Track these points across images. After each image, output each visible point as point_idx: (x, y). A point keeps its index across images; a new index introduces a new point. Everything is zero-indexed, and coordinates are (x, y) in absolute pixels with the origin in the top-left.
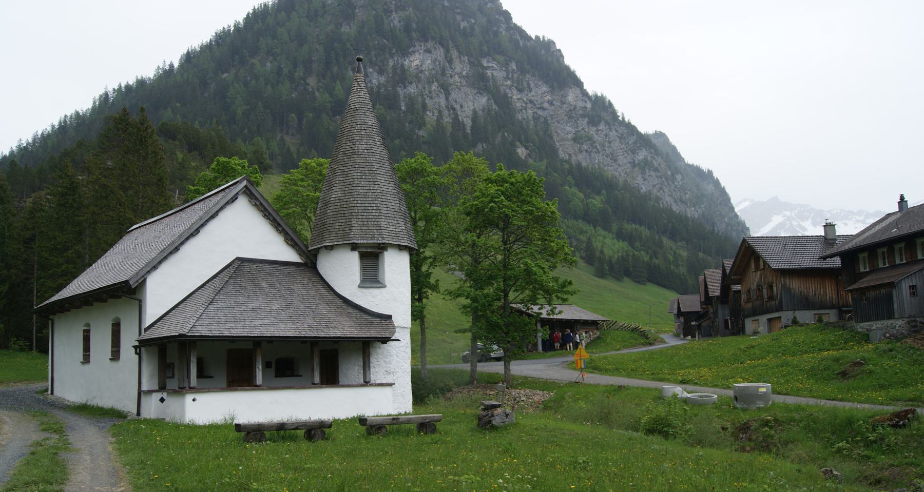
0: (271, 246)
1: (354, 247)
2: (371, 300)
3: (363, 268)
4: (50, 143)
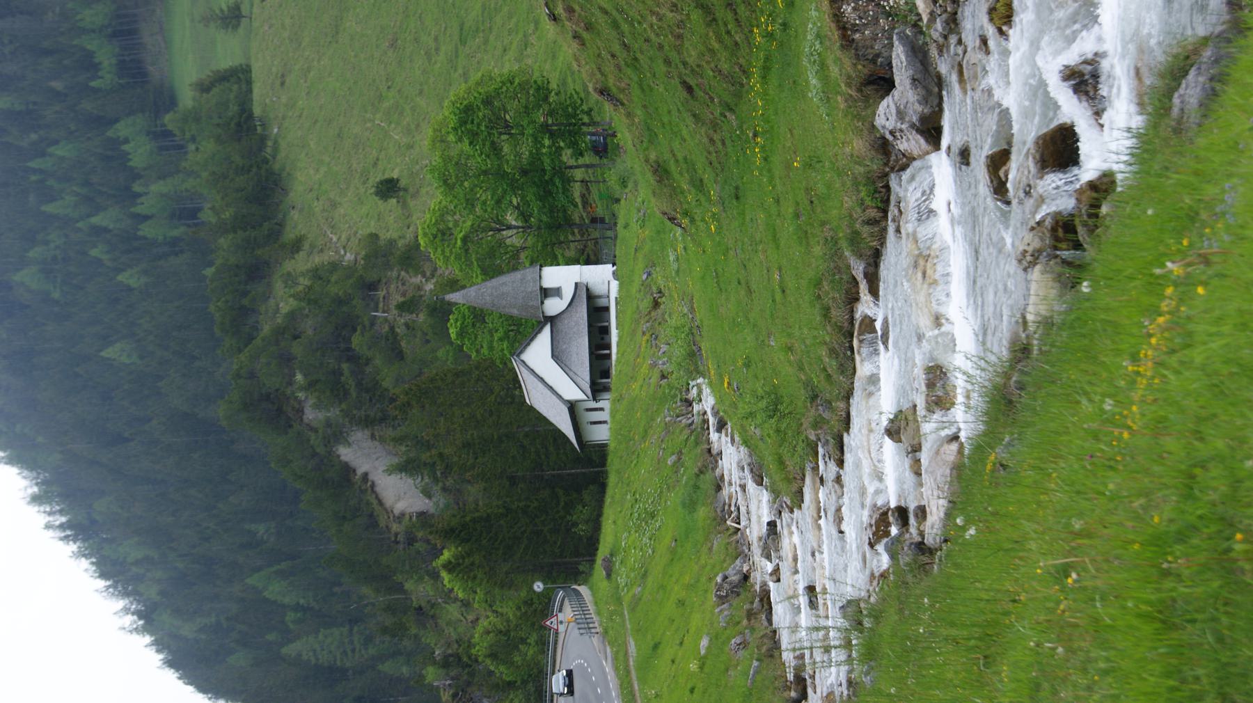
0: (543, 341)
2: (568, 293)
4: (132, 550)
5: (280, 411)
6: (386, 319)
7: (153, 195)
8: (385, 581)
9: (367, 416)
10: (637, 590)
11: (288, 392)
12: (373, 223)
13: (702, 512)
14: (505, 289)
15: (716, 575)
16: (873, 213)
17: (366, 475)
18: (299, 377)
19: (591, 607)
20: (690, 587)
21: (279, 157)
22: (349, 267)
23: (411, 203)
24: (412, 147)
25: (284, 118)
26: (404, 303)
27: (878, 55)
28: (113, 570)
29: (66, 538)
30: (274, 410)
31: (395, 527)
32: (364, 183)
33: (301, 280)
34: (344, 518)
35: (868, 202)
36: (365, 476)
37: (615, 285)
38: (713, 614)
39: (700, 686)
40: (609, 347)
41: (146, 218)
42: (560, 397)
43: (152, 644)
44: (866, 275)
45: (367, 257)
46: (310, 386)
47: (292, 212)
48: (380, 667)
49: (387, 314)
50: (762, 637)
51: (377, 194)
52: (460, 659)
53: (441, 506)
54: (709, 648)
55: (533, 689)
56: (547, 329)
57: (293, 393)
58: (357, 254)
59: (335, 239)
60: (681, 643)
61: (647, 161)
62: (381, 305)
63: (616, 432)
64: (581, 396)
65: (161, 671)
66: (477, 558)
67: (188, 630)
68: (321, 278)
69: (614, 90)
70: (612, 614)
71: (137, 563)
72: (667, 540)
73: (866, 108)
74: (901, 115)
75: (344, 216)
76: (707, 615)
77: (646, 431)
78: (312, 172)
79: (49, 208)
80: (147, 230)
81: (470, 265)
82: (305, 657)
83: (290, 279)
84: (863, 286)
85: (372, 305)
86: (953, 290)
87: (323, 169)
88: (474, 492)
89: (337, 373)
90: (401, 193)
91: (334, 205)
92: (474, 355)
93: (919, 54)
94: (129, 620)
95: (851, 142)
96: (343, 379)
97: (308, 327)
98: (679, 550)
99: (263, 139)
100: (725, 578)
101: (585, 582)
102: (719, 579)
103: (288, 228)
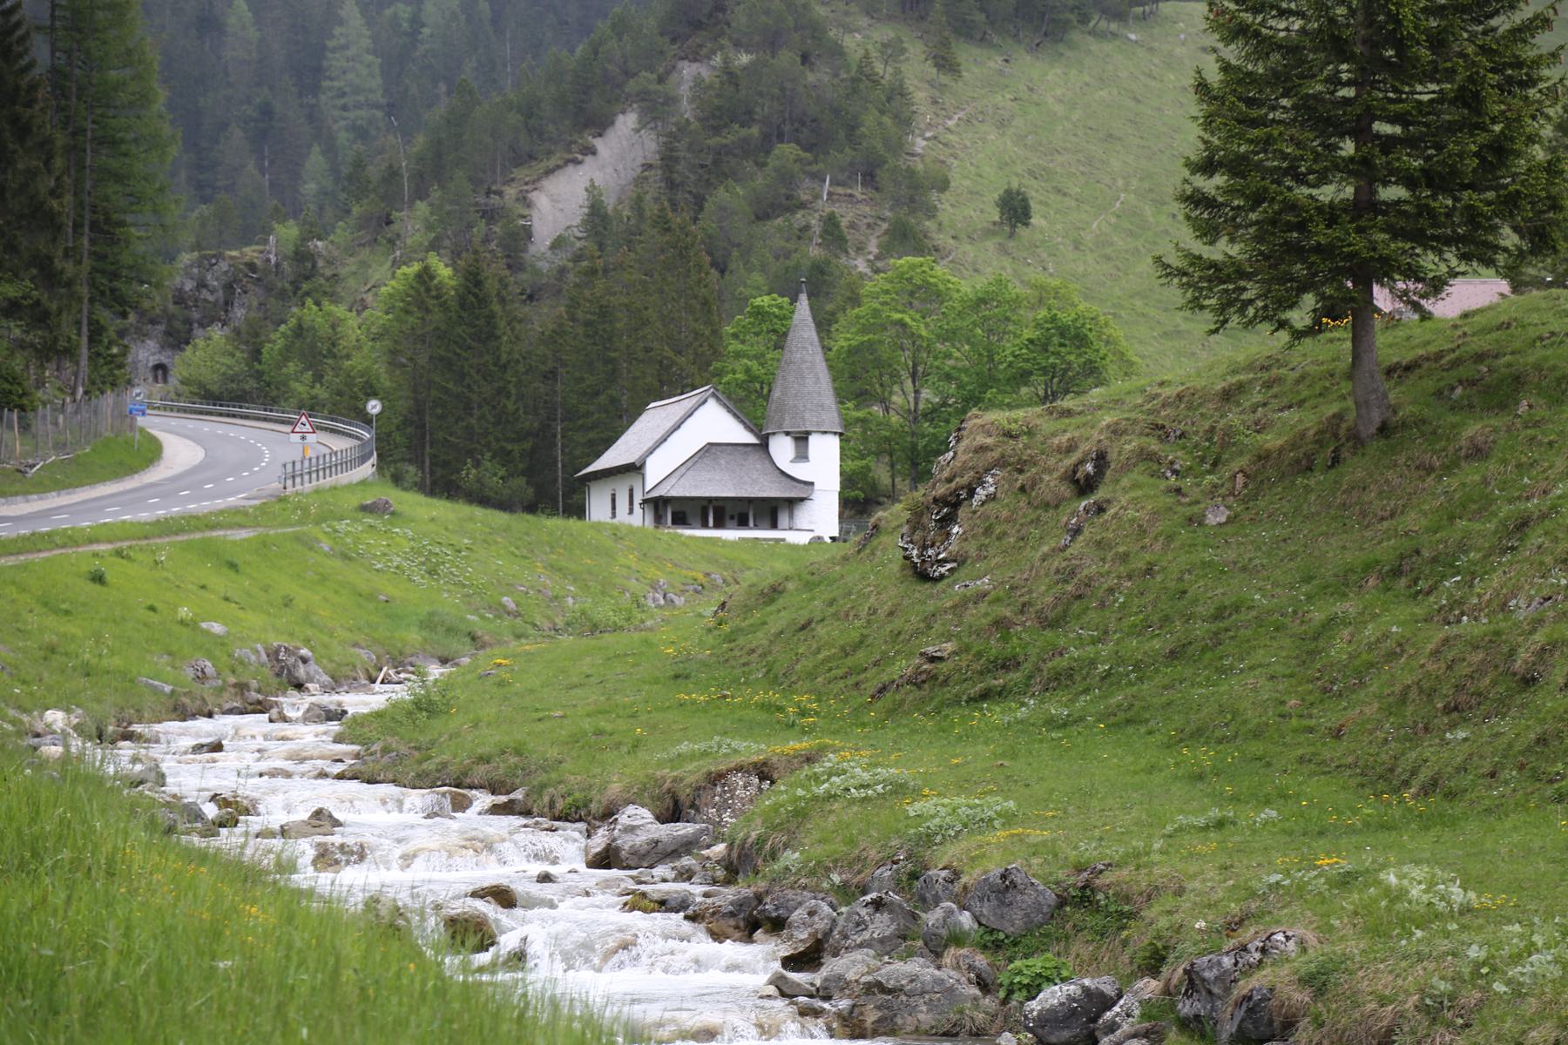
0: (735, 432)
1: (787, 434)
2: (799, 471)
3: (797, 447)
5: (697, 25)
6: (817, 197)
8: (432, 171)
9: (677, 160)
10: (325, 545)
11: (724, 41)
12: (967, 183)
13: (414, 636)
14: (810, 381)
15: (311, 649)
16: (560, 805)
17: (592, 152)
18: (745, 59)
19: (327, 482)
20: (307, 618)
21: (1090, 39)
22: (901, 145)
23: (991, 244)
24: (1077, 248)
25: (1151, 49)
26: (837, 225)
27: (698, 810)
31: (511, 192)
32: (1031, 173)
33: (890, 70)
34: (530, 115)
35: (570, 800)
36: (591, 151)
37: (801, 538)
38: (258, 640)
39: (154, 618)
40: (719, 524)
42: (651, 451)
44: (511, 801)
45: (911, 173)
46: (730, 76)
47: (999, 59)
48: (316, 149)
50: (203, 699)
51: (1008, 192)
52: (307, 278)
53: (540, 264)
54: (207, 633)
55: (247, 387)
56: (750, 439)
57: (722, 48)
58: (922, 156)
59: (950, 123)
60: (227, 599)
61: (787, 578)
62: (840, 190)
63: (599, 527)
64: (649, 485)
66: (437, 317)
68: (889, 100)
69: (875, 542)
70: (305, 510)
72: (389, 589)
73: (652, 798)
74: (631, 829)
75: (984, 140)
76: (255, 634)
77: (560, 570)
78: (1058, 92)
81: (864, 330)
82: (337, 31)
83: (893, 51)
84: (503, 799)
85: (841, 177)
86: (413, 852)
87: (1059, 109)
88: (543, 317)
89: (747, 118)
90: (1007, 229)
91: (1002, 124)
92: (729, 329)
93: (687, 846)
95: (620, 780)
96: (736, 127)
97: (818, 75)
98: (371, 606)
100: (305, 660)
101: (379, 469)
102: (304, 652)
103: (976, 51)
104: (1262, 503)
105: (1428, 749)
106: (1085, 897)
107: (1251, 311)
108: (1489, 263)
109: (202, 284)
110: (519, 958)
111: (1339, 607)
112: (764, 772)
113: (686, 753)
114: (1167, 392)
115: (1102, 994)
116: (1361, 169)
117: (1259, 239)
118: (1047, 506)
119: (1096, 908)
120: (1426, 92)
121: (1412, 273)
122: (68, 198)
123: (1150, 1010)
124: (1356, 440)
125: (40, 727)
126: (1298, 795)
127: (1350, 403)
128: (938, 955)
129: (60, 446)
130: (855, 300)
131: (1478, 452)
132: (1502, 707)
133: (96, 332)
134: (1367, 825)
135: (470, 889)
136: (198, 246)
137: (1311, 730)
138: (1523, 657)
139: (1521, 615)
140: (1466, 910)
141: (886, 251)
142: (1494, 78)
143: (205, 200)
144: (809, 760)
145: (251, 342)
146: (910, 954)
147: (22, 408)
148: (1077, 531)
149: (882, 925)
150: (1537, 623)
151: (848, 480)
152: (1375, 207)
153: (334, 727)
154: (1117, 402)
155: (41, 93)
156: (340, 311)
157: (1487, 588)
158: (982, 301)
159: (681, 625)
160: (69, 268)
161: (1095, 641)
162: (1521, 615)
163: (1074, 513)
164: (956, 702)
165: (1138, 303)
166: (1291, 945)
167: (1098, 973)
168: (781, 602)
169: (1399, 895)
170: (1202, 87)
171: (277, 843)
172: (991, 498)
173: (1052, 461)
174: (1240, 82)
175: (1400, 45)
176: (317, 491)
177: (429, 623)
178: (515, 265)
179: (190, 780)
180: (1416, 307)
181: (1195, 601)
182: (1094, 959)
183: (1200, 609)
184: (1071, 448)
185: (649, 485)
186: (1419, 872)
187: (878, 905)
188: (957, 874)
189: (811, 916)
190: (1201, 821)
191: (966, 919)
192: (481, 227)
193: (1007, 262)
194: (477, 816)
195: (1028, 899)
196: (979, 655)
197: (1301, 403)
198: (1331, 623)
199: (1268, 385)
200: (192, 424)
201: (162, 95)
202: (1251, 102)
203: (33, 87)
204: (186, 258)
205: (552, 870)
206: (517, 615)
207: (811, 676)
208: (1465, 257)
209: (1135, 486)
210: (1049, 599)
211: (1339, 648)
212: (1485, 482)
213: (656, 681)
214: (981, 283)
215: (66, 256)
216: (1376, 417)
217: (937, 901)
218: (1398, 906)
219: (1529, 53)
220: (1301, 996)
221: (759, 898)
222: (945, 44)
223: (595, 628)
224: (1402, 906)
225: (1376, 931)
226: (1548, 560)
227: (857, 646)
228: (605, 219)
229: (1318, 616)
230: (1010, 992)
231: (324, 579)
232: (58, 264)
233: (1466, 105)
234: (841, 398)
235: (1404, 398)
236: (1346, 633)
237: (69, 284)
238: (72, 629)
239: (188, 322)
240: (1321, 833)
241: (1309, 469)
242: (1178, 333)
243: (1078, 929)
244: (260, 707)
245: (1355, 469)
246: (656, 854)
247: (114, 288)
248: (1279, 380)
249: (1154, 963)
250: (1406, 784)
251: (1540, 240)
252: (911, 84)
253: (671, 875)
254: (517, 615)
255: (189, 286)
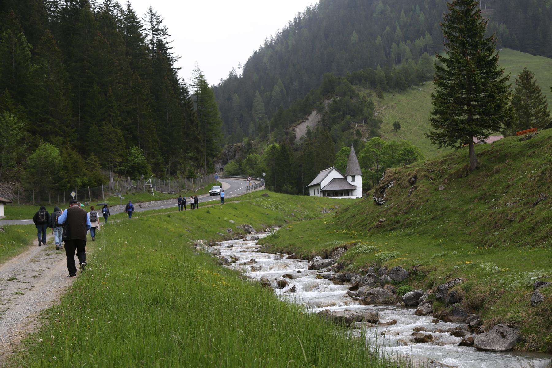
0: (340, 176)
2: (353, 183)
6: (355, 126)
7: (406, 47)
13: (273, 222)
14: (355, 164)
16: (302, 256)
17: (308, 119)
18: (338, 98)
19: (255, 190)
20: (251, 219)
23: (392, 134)
28: (286, 34)
29: (295, 19)
30: (329, 90)
31: (291, 129)
37: (355, 198)
39: (220, 220)
40: (337, 196)
41: (398, 45)
42: (322, 181)
43: (261, 48)
45: (375, 120)
46: (335, 102)
49: (356, 126)
51: (395, 123)
56: (342, 177)
64: (322, 188)
65: (277, 30)
67: (265, 60)
70: (250, 196)
71: (287, 43)
72: (268, 212)
74: (317, 261)
76: (240, 222)
79: (403, 12)
80: (394, 45)
81: (366, 153)
83: (369, 95)
87: (406, 105)
88: (298, 154)
91: (393, 109)
93: (329, 264)
94: (269, 40)
97: (354, 101)
99: (417, 85)
101: (266, 187)
104: (451, 185)
105: (490, 237)
106: (415, 272)
107: (446, 144)
108: (498, 131)
109: (229, 151)
110: (293, 290)
111: (469, 207)
112: (345, 248)
113: (329, 244)
114: (429, 162)
115: (419, 293)
116: (469, 112)
117: (447, 128)
118: (404, 188)
119: (417, 275)
120: (482, 95)
121: (482, 134)
122: (201, 135)
123: (430, 297)
124: (471, 170)
125: (197, 243)
126: (461, 248)
127: (469, 162)
128: (383, 286)
129: (201, 186)
130: (364, 147)
131: (498, 172)
132: (506, 227)
133: (208, 162)
134: (477, 254)
135: (283, 275)
136: (228, 144)
137: (464, 234)
138: (510, 215)
139: (509, 206)
140: (499, 272)
141: (370, 136)
142: (497, 91)
143: (230, 134)
144: (355, 245)
145: (239, 162)
146: (377, 286)
147: (194, 178)
148: (411, 193)
149: (371, 280)
150: (513, 208)
151: (364, 185)
152: (473, 120)
153: (256, 241)
154: (419, 165)
155: (195, 114)
156: (257, 155)
157: (501, 201)
158: (390, 146)
159: (328, 217)
160: (202, 149)
161: (416, 216)
162: (509, 206)
163: (410, 189)
164: (386, 231)
165: (424, 145)
166: (460, 281)
167: (418, 289)
168: (349, 211)
169: (484, 269)
170: (433, 96)
171: (242, 266)
172: (392, 187)
173: (405, 178)
174: (441, 95)
175: (476, 85)
176: (253, 192)
177: (276, 219)
178: (292, 144)
179: (226, 253)
180: (483, 141)
181: (437, 207)
182: (417, 286)
183: (439, 209)
184: (409, 175)
185: (322, 188)
186: (488, 264)
187: (370, 276)
188: (387, 268)
189: (356, 278)
190: (440, 255)
191: (389, 278)
192: (285, 136)
193: (396, 137)
194: (285, 259)
195: (402, 273)
196: (391, 221)
197: (459, 163)
198: (467, 210)
199: (451, 160)
200: (228, 180)
201: (220, 114)
202: (444, 99)
203: (194, 113)
204: (226, 146)
205: (300, 270)
206: (295, 216)
207: (355, 226)
208: (493, 130)
209: (423, 182)
210: (406, 208)
211: (469, 215)
212: (500, 178)
213: (322, 229)
214: (390, 142)
215: (201, 147)
216: (475, 165)
217: (383, 274)
218: (484, 272)
219: (504, 86)
220: (463, 293)
221: (344, 275)
222: (380, 93)
223: (310, 218)
224: (485, 272)
225: (479, 277)
226: (514, 194)
227: (365, 220)
228: (311, 133)
229: (464, 209)
230: (399, 294)
231: (254, 210)
232: (200, 148)
233: (491, 97)
234: (361, 167)
235: (481, 161)
236: (471, 212)
237: (202, 153)
238: (203, 223)
239: (227, 159)
240: (467, 256)
241: (461, 177)
242: (433, 150)
243: (414, 279)
244: (242, 238)
245: (471, 177)
246: (323, 266)
247: (211, 153)
248: (454, 158)
249: (430, 286)
250: (485, 244)
251: (508, 125)
252: (373, 101)
253: (326, 270)
254: (295, 216)
255: (227, 152)
